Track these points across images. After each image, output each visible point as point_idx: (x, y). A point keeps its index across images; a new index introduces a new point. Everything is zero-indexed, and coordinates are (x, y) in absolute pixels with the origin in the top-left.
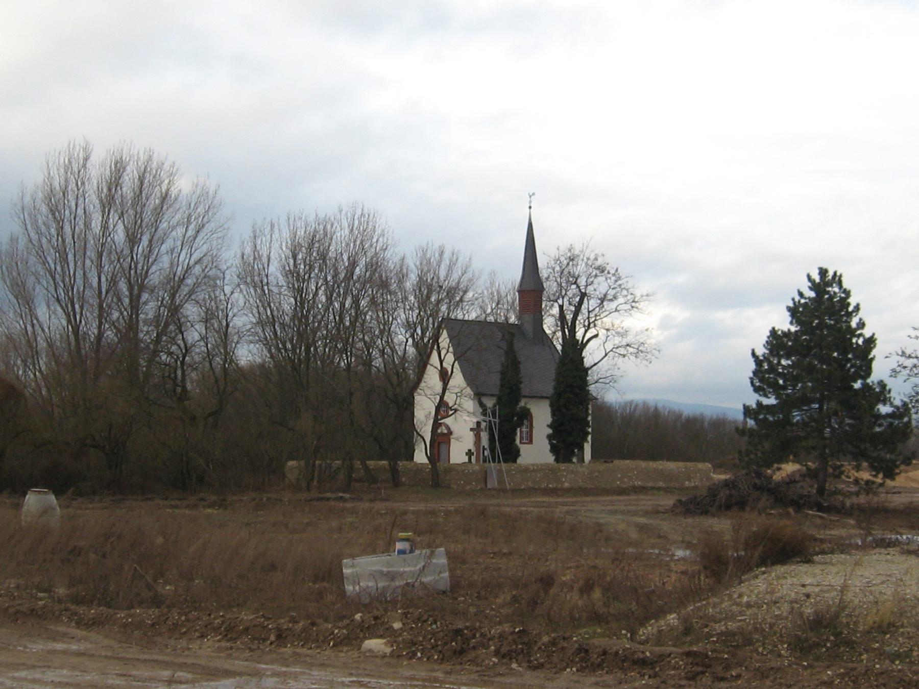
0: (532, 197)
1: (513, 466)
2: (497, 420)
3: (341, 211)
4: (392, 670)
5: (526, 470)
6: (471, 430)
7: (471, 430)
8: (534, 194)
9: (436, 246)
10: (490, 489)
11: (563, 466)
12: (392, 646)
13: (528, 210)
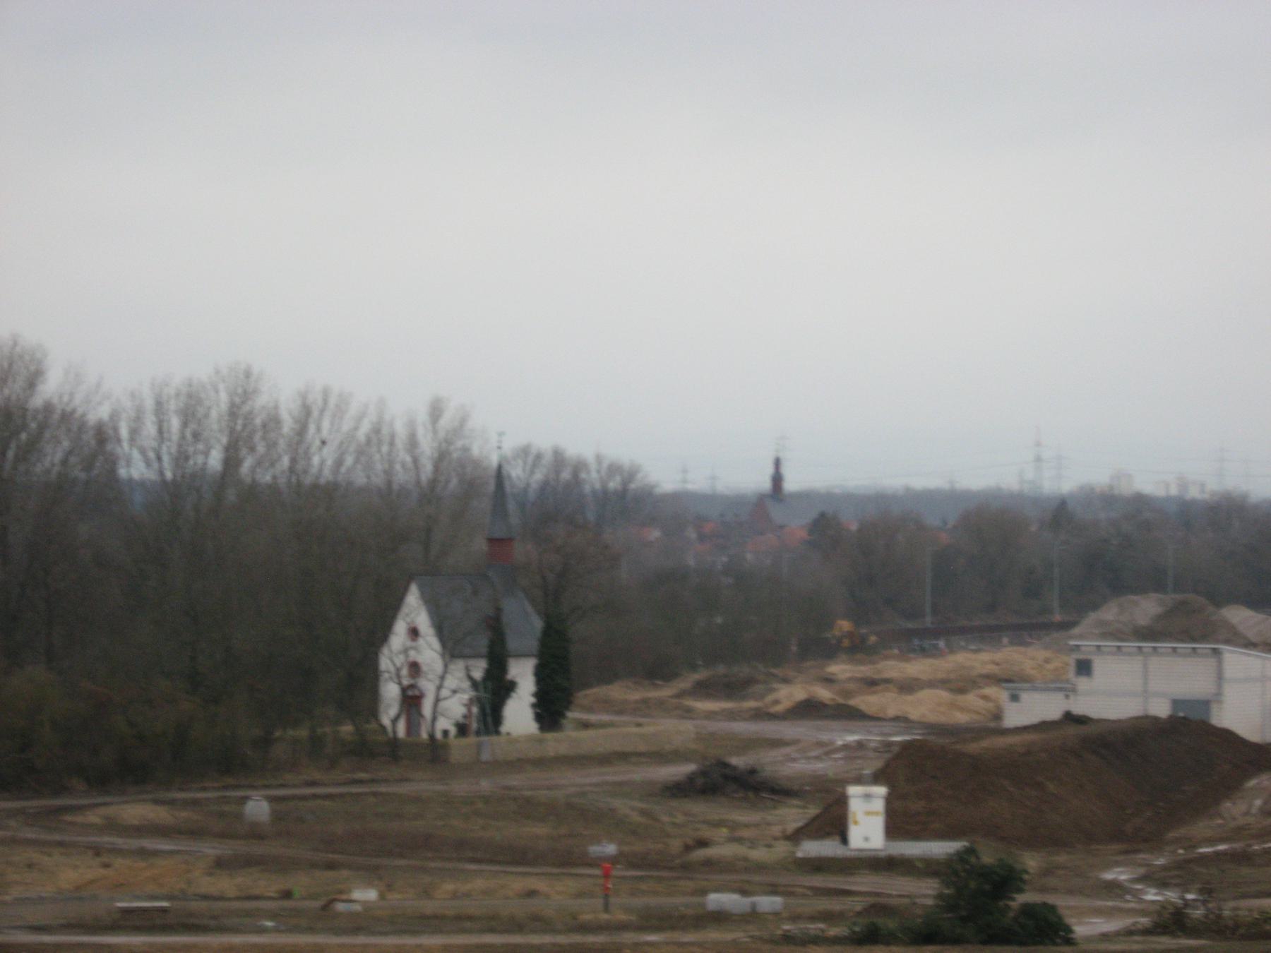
1: (494, 739)
11: (550, 736)
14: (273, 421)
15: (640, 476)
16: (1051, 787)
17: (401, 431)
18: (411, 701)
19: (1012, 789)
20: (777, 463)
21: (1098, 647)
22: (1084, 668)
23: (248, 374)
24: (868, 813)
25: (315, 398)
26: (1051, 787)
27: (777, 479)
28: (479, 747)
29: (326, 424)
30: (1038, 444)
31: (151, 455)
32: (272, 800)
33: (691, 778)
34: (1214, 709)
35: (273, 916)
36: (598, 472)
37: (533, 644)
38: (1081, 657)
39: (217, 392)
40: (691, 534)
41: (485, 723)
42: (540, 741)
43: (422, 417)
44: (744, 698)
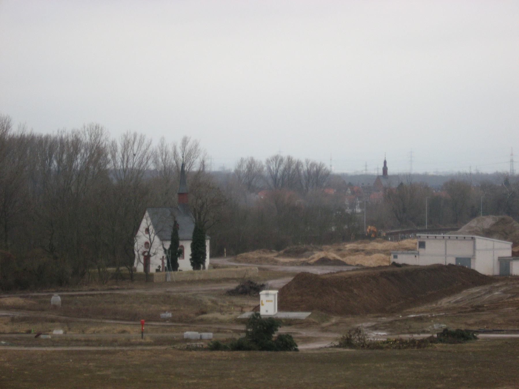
1: (176, 273)
2: (170, 256)
3: (84, 127)
6: (161, 259)
7: (161, 259)
9: (132, 133)
10: (168, 282)
11: (196, 271)
12: (371, 223)
15: (324, 168)
16: (355, 291)
17: (171, 150)
19: (337, 292)
20: (385, 162)
22: (422, 245)
26: (355, 291)
27: (385, 169)
29: (135, 147)
30: (512, 155)
32: (61, 296)
33: (237, 289)
35: (5, 339)
36: (307, 166)
37: (191, 235)
38: (422, 240)
39: (85, 135)
40: (349, 191)
44: (302, 257)
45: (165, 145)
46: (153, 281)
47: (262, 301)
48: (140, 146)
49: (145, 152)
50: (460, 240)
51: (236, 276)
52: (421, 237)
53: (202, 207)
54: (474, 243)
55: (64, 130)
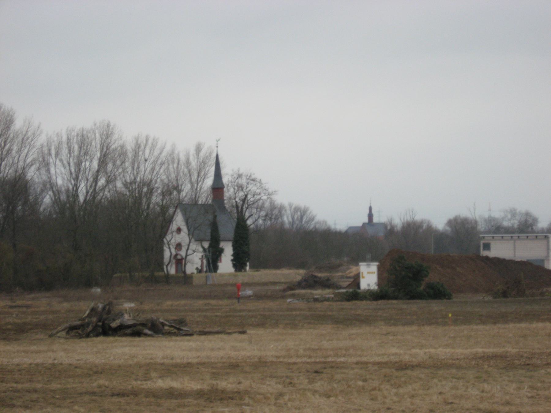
0: (218, 142)
1: (214, 274)
2: (211, 254)
3: (95, 125)
4: (330, 359)
5: (222, 275)
6: (200, 259)
7: (200, 259)
8: (219, 140)
11: (239, 273)
13: (219, 145)
14: (123, 154)
16: (458, 269)
17: (183, 158)
18: (180, 262)
19: (440, 269)
20: (370, 209)
21: (493, 237)
23: (108, 126)
24: (368, 273)
25: (142, 140)
26: (458, 269)
27: (370, 216)
28: (207, 278)
30: (490, 210)
31: (65, 162)
34: (546, 262)
36: (290, 210)
38: (486, 242)
41: (209, 268)
42: (235, 276)
43: (192, 151)
45: (176, 152)
46: (192, 283)
47: (362, 273)
48: (152, 151)
49: (158, 158)
50: (533, 239)
51: (283, 280)
52: (485, 238)
53: (244, 200)
54: (548, 242)
55: (74, 129)
